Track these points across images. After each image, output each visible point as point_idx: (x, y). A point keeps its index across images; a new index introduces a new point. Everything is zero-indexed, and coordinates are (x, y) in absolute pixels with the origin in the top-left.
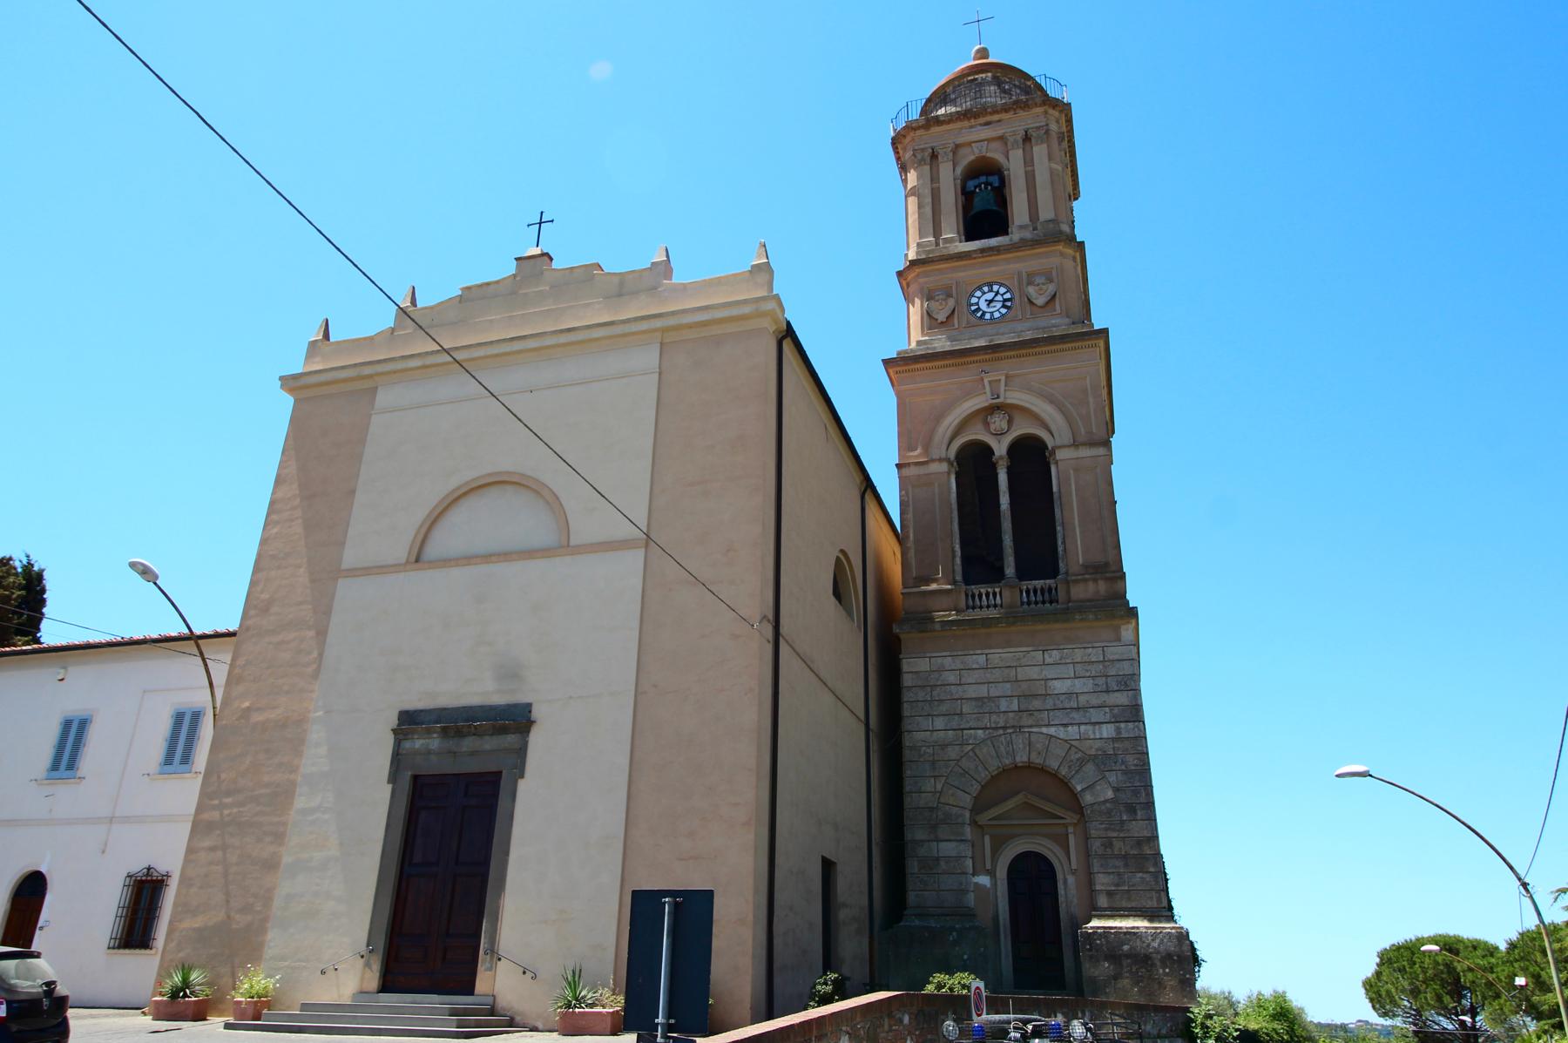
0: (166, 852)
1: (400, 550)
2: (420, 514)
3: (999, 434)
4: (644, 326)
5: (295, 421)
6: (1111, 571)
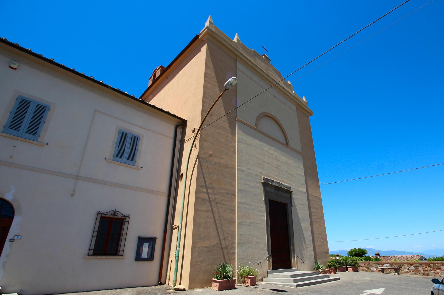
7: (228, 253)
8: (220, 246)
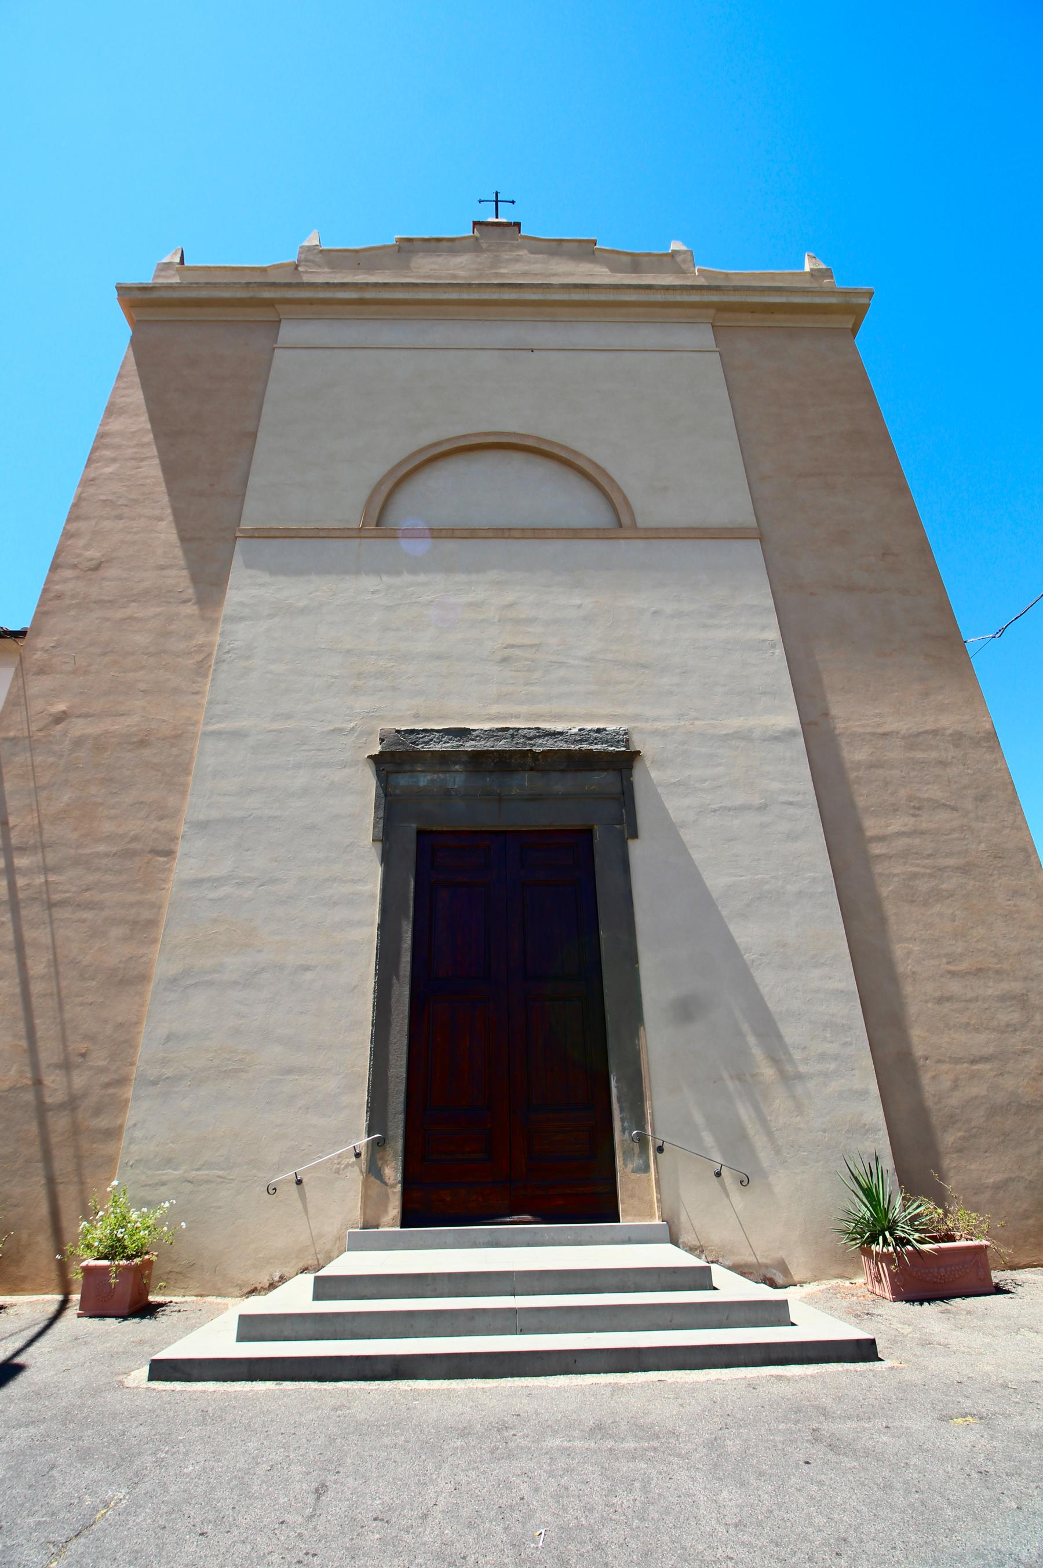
1: (349, 509)
4: (695, 298)
7: (76, 1130)
8: (29, 1097)
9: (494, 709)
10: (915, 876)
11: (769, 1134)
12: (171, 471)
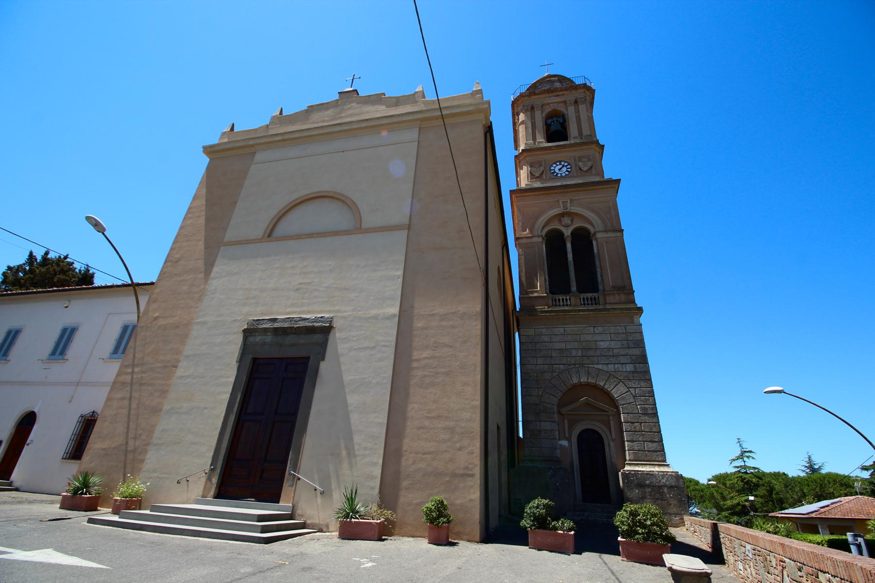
0: (93, 400)
1: (259, 231)
2: (273, 212)
3: (567, 226)
4: (411, 117)
5: (209, 169)
6: (626, 289)
8: (124, 448)
9: (289, 310)
10: (426, 376)
11: (338, 479)
12: (208, 220)
